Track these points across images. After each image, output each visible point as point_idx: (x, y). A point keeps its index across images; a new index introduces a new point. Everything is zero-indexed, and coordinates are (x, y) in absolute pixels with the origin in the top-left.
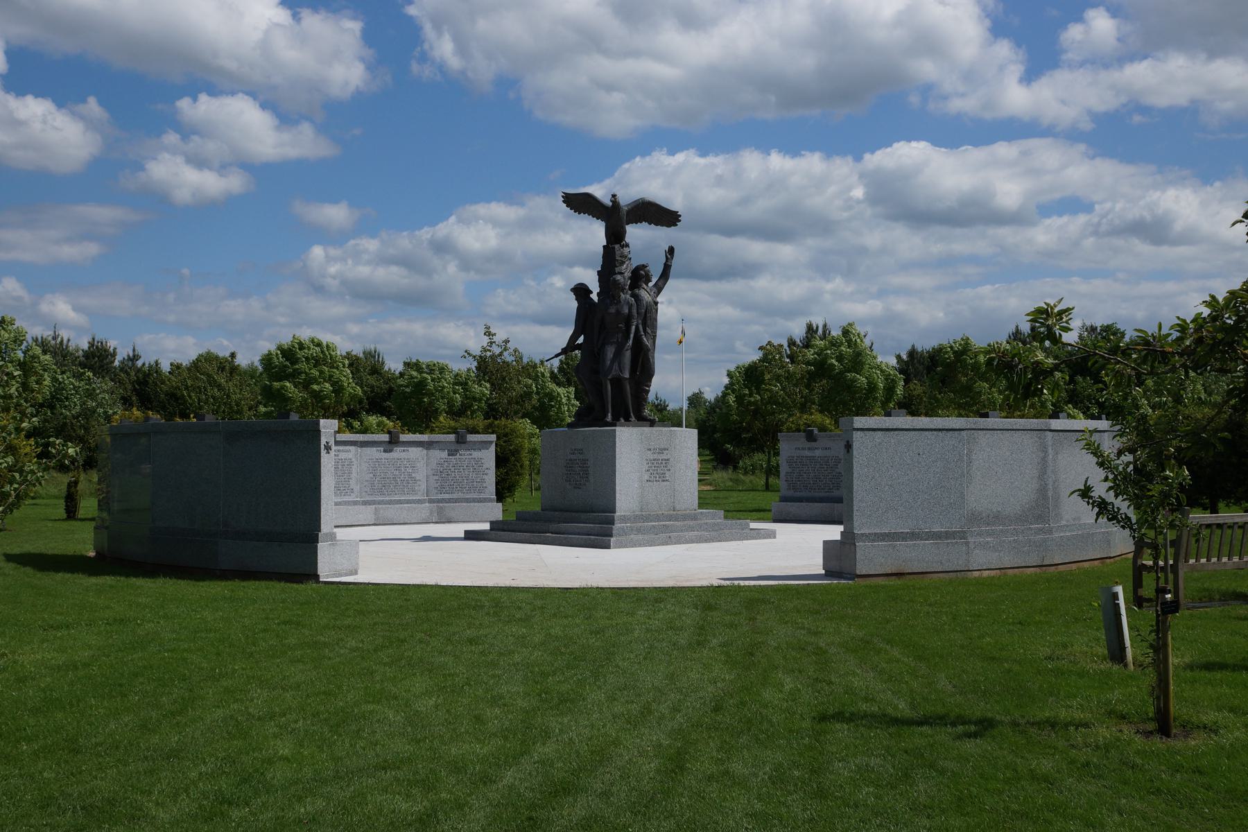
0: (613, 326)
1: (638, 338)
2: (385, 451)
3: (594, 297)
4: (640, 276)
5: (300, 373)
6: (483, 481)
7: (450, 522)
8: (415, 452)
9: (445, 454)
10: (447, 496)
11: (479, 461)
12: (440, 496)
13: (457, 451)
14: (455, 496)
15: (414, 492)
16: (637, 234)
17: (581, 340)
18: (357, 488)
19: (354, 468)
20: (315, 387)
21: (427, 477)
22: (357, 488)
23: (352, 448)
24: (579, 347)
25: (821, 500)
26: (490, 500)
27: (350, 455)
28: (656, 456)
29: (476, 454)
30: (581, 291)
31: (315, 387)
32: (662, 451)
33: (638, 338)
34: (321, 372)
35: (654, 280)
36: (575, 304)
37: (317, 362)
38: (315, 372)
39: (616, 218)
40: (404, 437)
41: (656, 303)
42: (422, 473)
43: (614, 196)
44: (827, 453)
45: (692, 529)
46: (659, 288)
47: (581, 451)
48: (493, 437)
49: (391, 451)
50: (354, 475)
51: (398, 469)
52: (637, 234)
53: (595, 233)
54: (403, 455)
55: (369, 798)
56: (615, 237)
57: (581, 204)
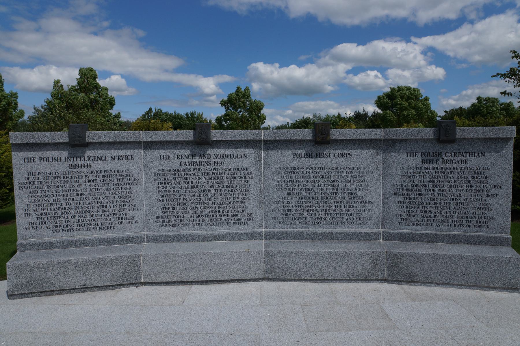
2: (309, 155)
5: (396, 105)
6: (487, 207)
8: (361, 157)
9: (416, 161)
10: (418, 230)
11: (480, 175)
12: (405, 230)
13: (439, 155)
14: (432, 231)
15: (360, 220)
18: (259, 213)
19: (253, 183)
20: (405, 113)
21: (385, 197)
22: (259, 213)
23: (250, 152)
26: (499, 242)
27: (245, 163)
29: (473, 162)
31: (405, 113)
34: (410, 104)
37: (408, 99)
38: (406, 104)
40: (92, 136)
42: (374, 191)
48: (511, 131)
49: (319, 155)
50: (253, 192)
51: (332, 184)
54: (340, 162)
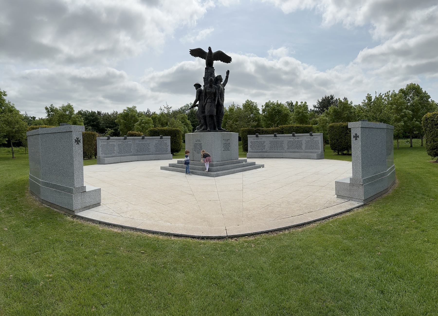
0: (211, 91)
1: (218, 101)
3: (202, 88)
4: (219, 78)
6: (167, 148)
7: (158, 160)
16: (216, 63)
17: (198, 103)
24: (197, 106)
25: (260, 152)
28: (226, 142)
30: (197, 86)
32: (228, 140)
33: (218, 101)
35: (223, 81)
36: (22, 113)
39: (211, 57)
41: (224, 89)
43: (210, 47)
44: (261, 140)
45: (239, 167)
46: (224, 84)
47: (199, 141)
52: (216, 63)
53: (201, 63)
54: (146, 142)
55: (190, 302)
56: (209, 65)
57: (197, 53)
